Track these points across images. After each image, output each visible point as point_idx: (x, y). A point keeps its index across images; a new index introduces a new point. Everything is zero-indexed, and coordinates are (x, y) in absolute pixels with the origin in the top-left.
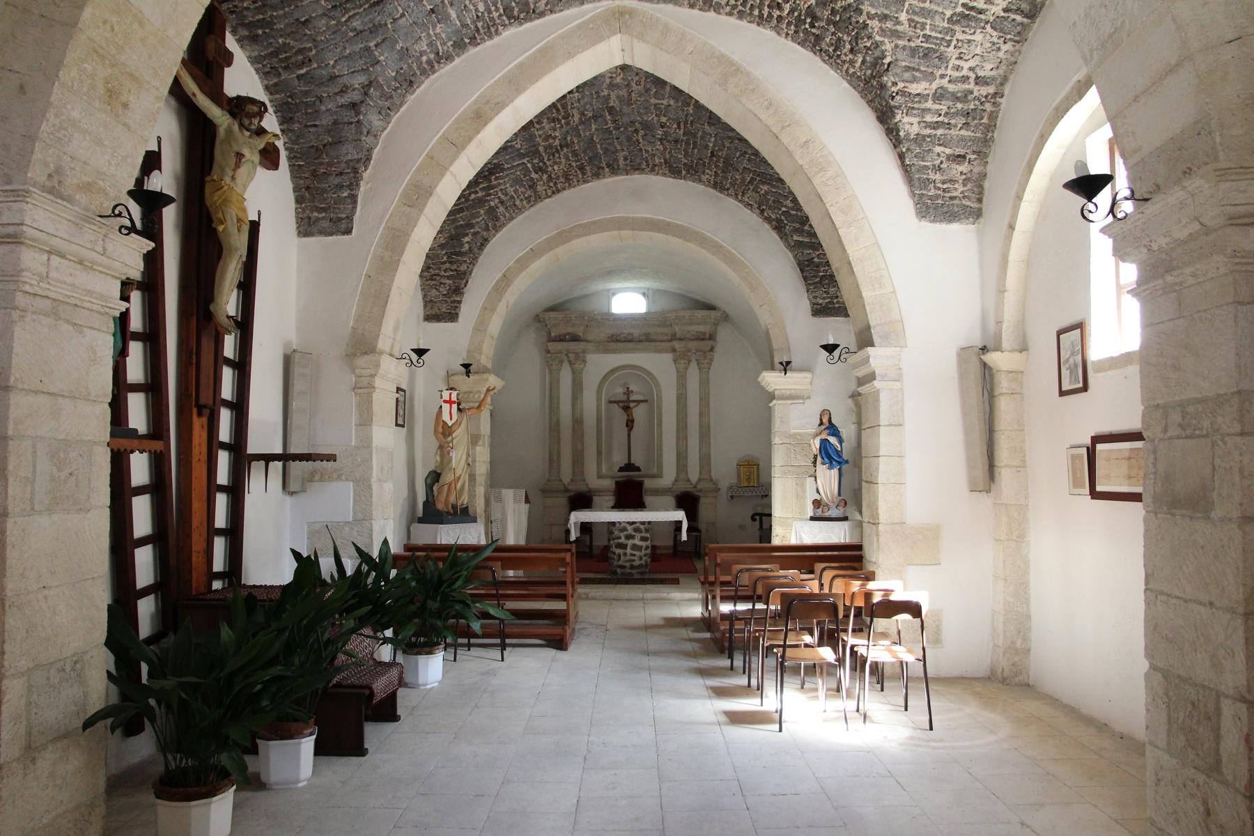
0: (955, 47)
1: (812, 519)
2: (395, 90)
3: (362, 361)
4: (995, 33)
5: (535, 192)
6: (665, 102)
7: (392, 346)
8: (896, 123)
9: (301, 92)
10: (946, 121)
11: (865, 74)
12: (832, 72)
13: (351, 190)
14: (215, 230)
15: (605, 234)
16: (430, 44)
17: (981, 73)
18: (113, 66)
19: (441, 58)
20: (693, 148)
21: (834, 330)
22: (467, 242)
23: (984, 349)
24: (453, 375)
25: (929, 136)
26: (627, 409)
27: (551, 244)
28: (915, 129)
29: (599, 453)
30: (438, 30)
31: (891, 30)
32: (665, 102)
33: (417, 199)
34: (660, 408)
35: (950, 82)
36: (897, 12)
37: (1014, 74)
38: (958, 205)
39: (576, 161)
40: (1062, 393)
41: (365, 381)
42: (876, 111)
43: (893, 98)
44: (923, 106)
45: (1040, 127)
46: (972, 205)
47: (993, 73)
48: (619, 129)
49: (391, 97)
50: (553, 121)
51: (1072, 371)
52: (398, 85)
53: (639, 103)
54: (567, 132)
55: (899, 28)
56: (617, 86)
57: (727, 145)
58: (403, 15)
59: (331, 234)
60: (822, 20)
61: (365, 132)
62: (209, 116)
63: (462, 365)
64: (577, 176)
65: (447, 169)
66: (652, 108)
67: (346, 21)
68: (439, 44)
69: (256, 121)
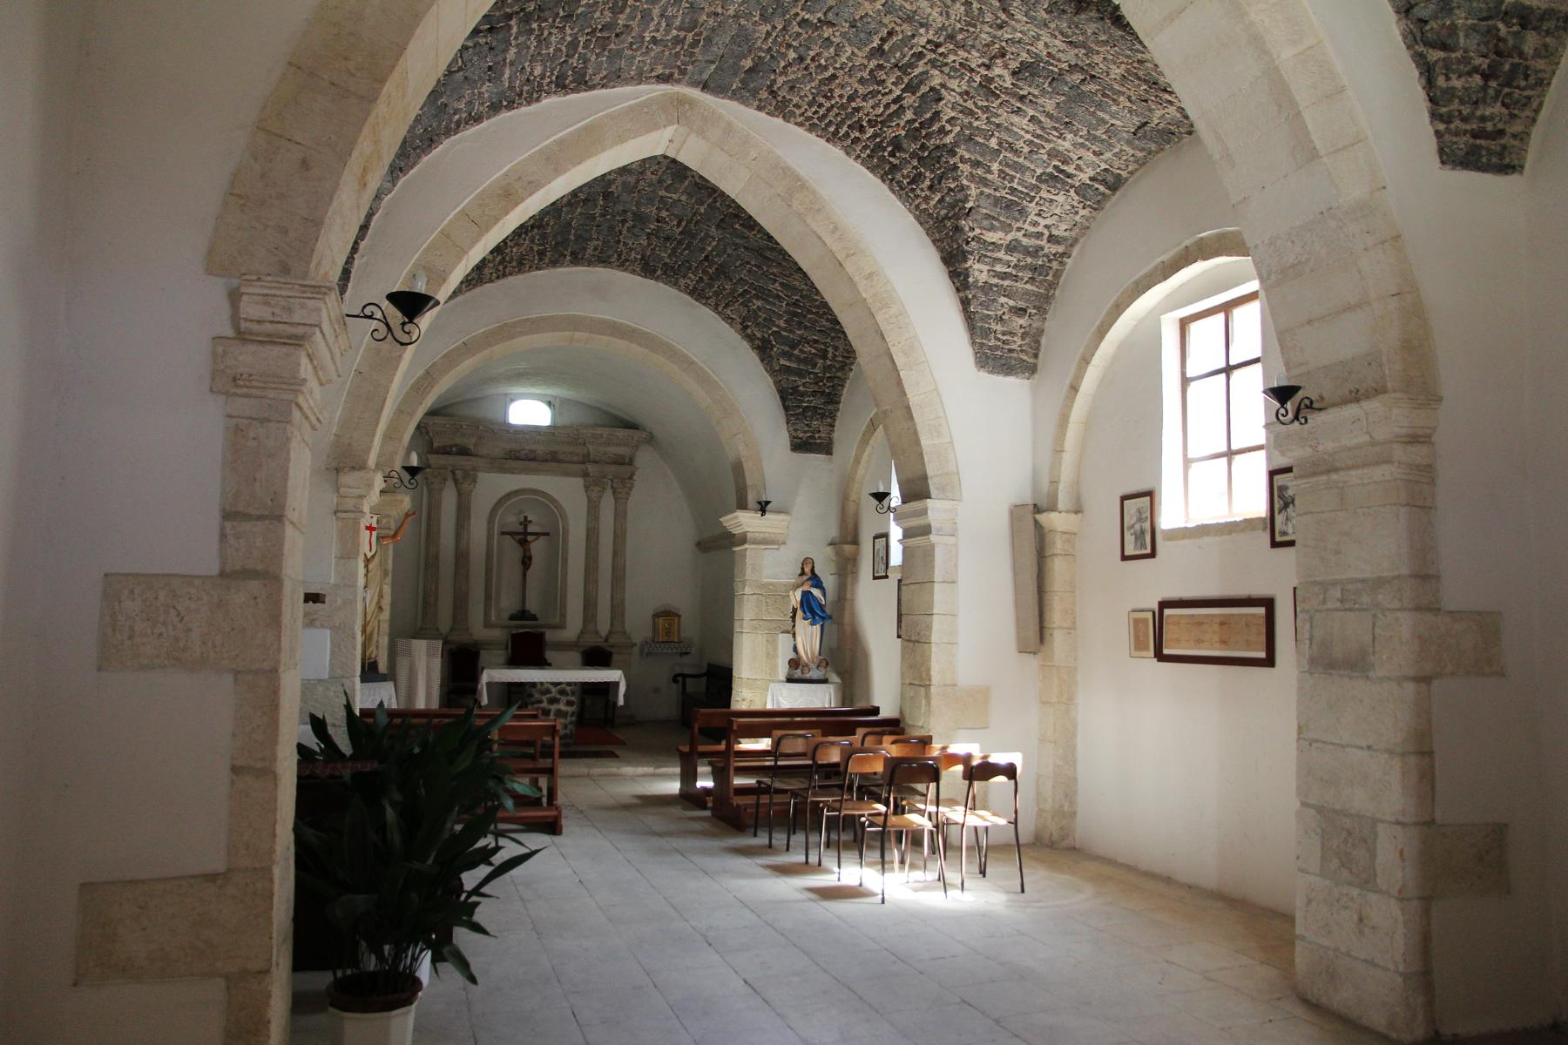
0: (1037, 204)
1: (790, 680)
3: (348, 478)
4: (1077, 198)
6: (675, 196)
8: (967, 269)
10: (1014, 273)
12: (899, 203)
17: (1055, 232)
20: (685, 249)
23: (1037, 509)
25: (996, 286)
26: (523, 543)
28: (983, 277)
29: (488, 597)
31: (980, 177)
32: (675, 196)
34: (565, 542)
35: (1024, 235)
38: (1015, 359)
40: (1124, 558)
41: (349, 503)
43: (968, 243)
44: (996, 255)
45: (1115, 298)
46: (1028, 360)
47: (1067, 234)
48: (605, 216)
53: (643, 192)
55: (989, 177)
60: (905, 151)
64: (533, 261)
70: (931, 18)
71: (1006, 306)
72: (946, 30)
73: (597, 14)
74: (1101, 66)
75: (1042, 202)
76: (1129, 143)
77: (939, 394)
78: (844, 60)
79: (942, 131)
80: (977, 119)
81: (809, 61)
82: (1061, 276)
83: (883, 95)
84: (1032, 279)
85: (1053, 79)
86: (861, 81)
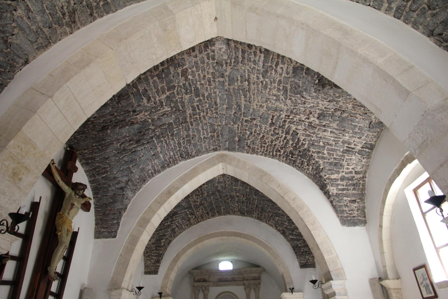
0: (346, 161)
2: (138, 183)
3: (114, 293)
4: (359, 156)
5: (190, 222)
6: (238, 188)
7: (128, 285)
8: (328, 190)
9: (103, 183)
10: (346, 188)
11: (313, 173)
12: (301, 173)
13: (118, 220)
14: (57, 235)
15: (217, 238)
16: (152, 167)
17: (356, 170)
18: (18, 163)
19: (156, 172)
20: (249, 205)
21: (311, 273)
22: (163, 242)
24: (154, 297)
25: (341, 194)
27: (195, 243)
28: (335, 192)
30: (156, 162)
31: (321, 157)
32: (238, 188)
33: (143, 224)
35: (345, 174)
36: (323, 150)
37: (369, 169)
38: (356, 219)
39: (205, 210)
42: (319, 186)
43: (325, 181)
45: (384, 187)
46: (362, 219)
47: (361, 170)
49: (136, 185)
50: (197, 195)
51: (426, 287)
52: (139, 181)
54: (202, 200)
55: (324, 156)
56: (221, 182)
57: (262, 203)
58: (143, 156)
59: (108, 238)
61: (125, 198)
62: (63, 189)
63: (158, 293)
64: (206, 216)
65: (156, 212)
66: (234, 190)
67: (122, 158)
68: (155, 167)
69: (81, 192)
70: (282, 108)
71: (347, 200)
72: (289, 110)
73: (182, 133)
74: (344, 106)
75: (347, 160)
76: (369, 131)
77: (329, 238)
78: (264, 130)
79: (303, 144)
80: (312, 137)
81: (254, 133)
82: (365, 185)
83: (280, 138)
84: (354, 189)
85: (331, 116)
86: (272, 135)
